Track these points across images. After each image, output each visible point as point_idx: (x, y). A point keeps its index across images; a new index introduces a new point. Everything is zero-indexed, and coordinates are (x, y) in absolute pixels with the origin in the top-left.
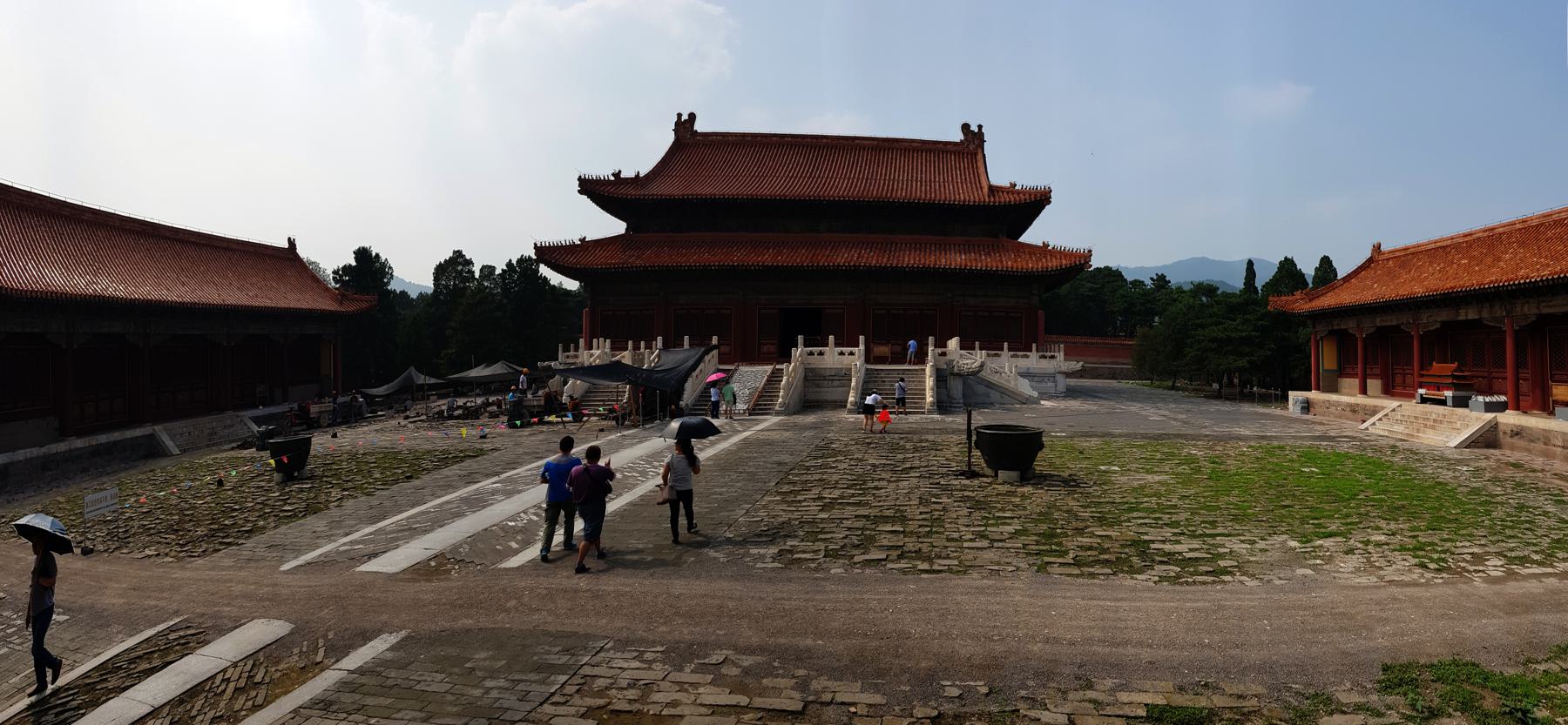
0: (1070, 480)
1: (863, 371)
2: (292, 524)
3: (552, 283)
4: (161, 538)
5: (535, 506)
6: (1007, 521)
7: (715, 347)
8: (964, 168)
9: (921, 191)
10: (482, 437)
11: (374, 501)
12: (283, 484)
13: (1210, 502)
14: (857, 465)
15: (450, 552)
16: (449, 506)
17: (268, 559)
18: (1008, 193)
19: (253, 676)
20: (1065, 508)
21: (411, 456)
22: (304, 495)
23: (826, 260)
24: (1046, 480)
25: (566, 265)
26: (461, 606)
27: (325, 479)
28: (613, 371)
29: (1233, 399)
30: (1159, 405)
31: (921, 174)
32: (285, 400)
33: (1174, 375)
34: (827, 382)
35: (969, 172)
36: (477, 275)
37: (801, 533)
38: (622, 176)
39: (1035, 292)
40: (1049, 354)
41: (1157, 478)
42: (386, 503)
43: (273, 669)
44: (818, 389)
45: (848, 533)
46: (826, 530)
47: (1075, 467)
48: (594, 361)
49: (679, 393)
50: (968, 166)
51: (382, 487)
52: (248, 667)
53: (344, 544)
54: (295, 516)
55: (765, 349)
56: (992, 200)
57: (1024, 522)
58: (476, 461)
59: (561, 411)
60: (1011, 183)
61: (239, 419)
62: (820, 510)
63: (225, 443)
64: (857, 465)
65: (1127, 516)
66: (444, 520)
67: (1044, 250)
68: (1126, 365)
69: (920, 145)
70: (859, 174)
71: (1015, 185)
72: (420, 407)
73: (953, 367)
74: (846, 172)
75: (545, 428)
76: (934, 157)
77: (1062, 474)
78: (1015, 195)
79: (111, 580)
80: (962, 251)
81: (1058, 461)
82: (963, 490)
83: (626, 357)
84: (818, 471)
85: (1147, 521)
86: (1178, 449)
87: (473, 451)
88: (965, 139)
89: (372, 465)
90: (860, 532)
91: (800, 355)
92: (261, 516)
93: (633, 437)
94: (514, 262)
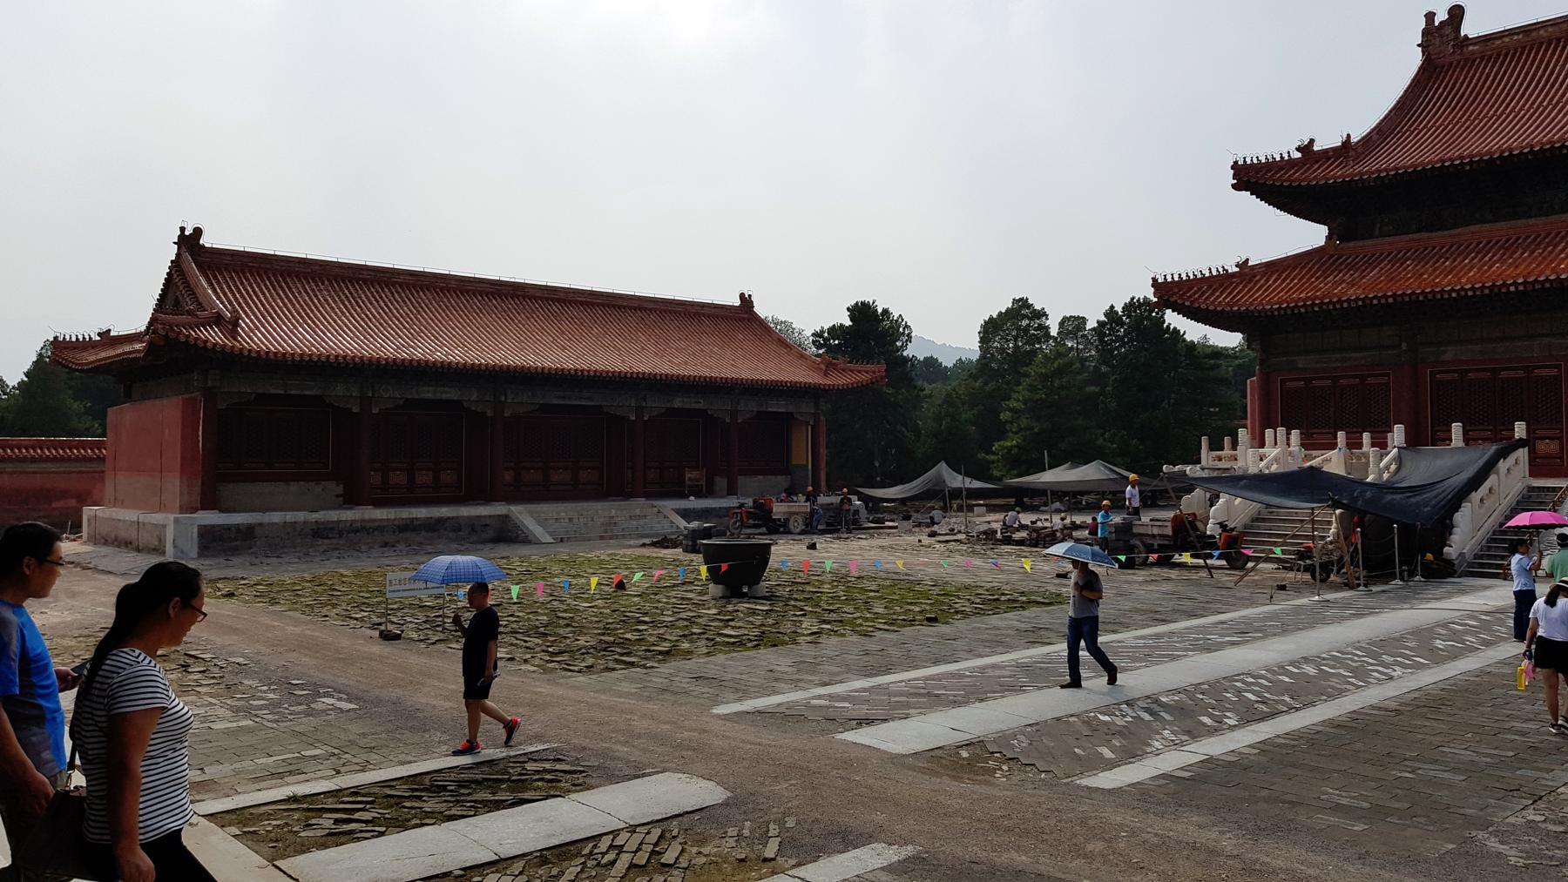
2: (734, 655)
3: (1188, 338)
4: (517, 639)
5: (1148, 697)
7: (1521, 443)
10: (1059, 576)
11: (872, 645)
12: (725, 601)
16: (998, 673)
17: (694, 693)
19: (659, 853)
21: (937, 590)
22: (758, 620)
25: (1212, 308)
26: (1008, 830)
27: (792, 603)
32: (731, 491)
36: (1054, 332)
42: (893, 651)
43: (695, 850)
49: (1443, 528)
51: (886, 627)
52: (654, 837)
53: (820, 697)
54: (741, 644)
61: (656, 509)
63: (631, 537)
66: (986, 692)
72: (956, 520)
75: (1174, 574)
79: (430, 676)
83: (1333, 462)
89: (872, 594)
92: (684, 636)
93: (1346, 605)
94: (1119, 309)
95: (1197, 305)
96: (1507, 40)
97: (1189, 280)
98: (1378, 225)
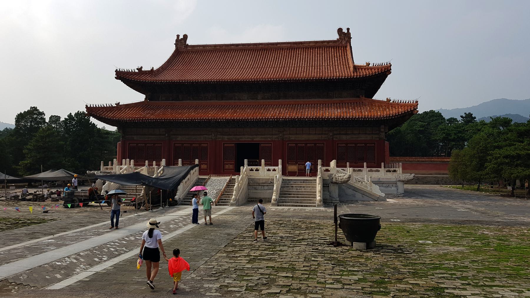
0: (398, 249)
1: (281, 180)
3: (98, 127)
5: (76, 254)
6: (354, 273)
7: (197, 165)
8: (339, 56)
9: (314, 73)
10: (44, 212)
13: (493, 265)
14: (272, 237)
15: (13, 278)
16: (16, 251)
18: (365, 69)
20: (392, 266)
23: (261, 116)
24: (383, 249)
25: (106, 117)
28: (135, 177)
29: (522, 197)
30: (466, 201)
31: (315, 62)
33: (479, 181)
34: (261, 187)
35: (342, 58)
36: (47, 120)
37: (235, 276)
38: (143, 70)
39: (382, 130)
40: (392, 169)
41: (456, 249)
44: (256, 191)
45: (261, 277)
46: (249, 274)
47: (404, 240)
48: (123, 172)
50: (342, 55)
55: (227, 167)
56: (355, 74)
57: (365, 274)
58: (39, 226)
59: (99, 200)
62: (247, 263)
64: (272, 237)
65: (432, 272)
66: (10, 260)
67: (388, 104)
68: (446, 174)
69: (314, 44)
70: (280, 65)
71: (369, 64)
73: (333, 178)
74: (273, 64)
75: (88, 209)
76: (322, 50)
77: (394, 245)
78: (370, 70)
80: (339, 108)
81: (392, 237)
82: (331, 254)
83: (144, 170)
84: (250, 240)
85: (445, 275)
86: (475, 230)
87: (37, 220)
88: (340, 38)
90: (267, 276)
91: (246, 171)
93: (145, 216)
94: (73, 114)
96: (198, 48)
97: (99, 107)
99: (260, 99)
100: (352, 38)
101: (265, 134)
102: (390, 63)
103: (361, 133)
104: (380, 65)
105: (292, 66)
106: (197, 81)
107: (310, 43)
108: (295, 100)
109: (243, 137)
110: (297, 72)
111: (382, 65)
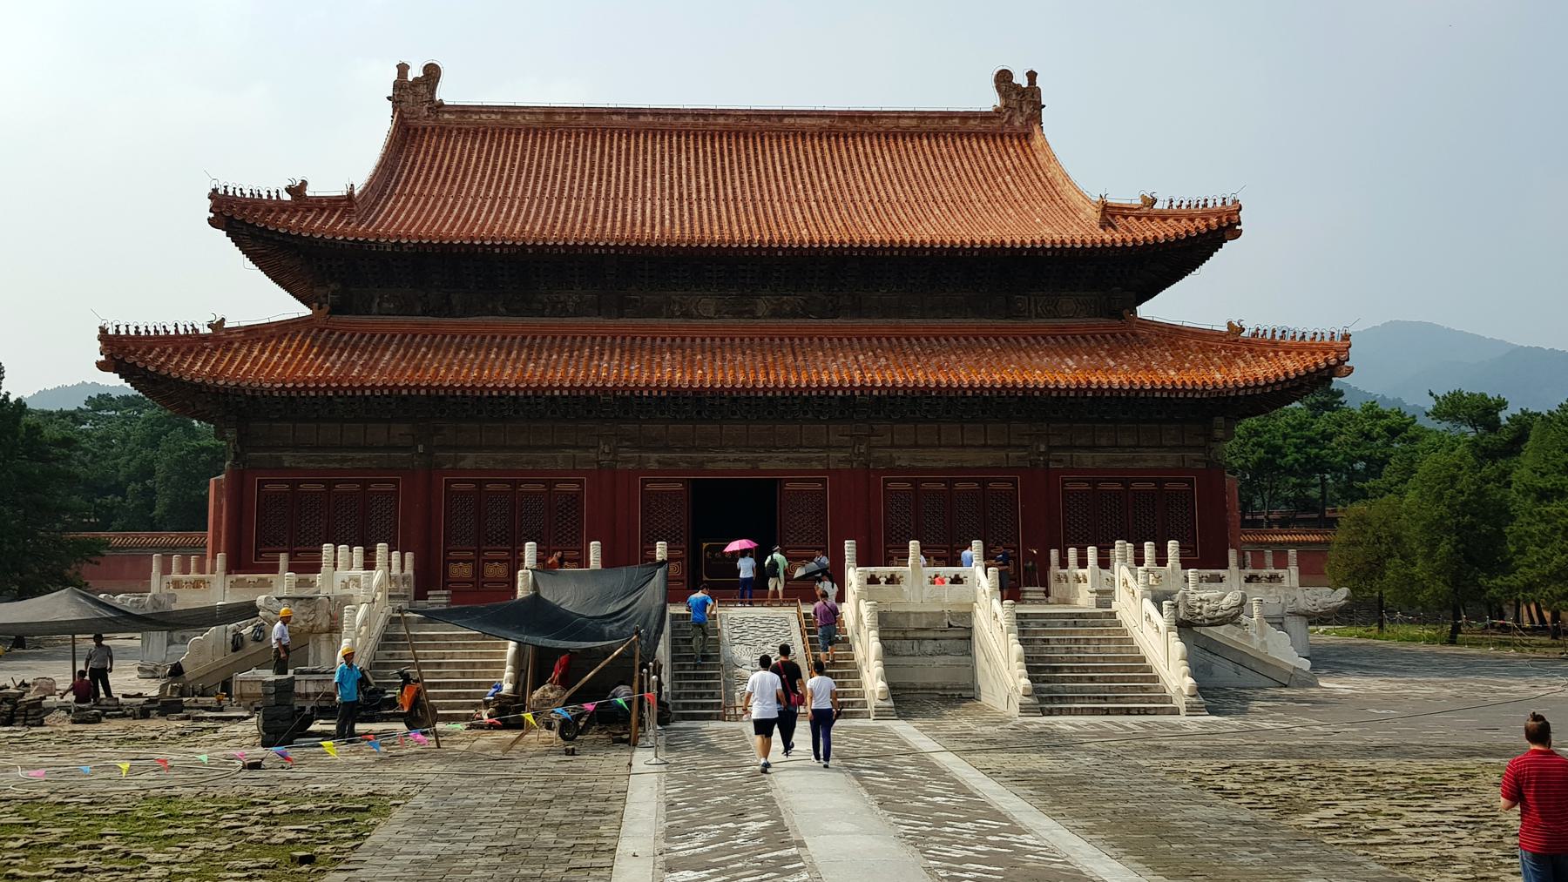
38: (308, 193)
60: (1144, 197)
69: (914, 122)
71: (1155, 201)
95: (166, 372)
96: (484, 116)
97: (148, 337)
98: (378, 300)
99: (765, 317)
100: (1044, 106)
101: (801, 446)
102: (1235, 202)
103: (1145, 444)
104: (1197, 206)
105: (514, 195)
106: (540, 243)
107: (899, 117)
108: (894, 321)
109: (721, 456)
110: (404, 214)
111: (1205, 205)
